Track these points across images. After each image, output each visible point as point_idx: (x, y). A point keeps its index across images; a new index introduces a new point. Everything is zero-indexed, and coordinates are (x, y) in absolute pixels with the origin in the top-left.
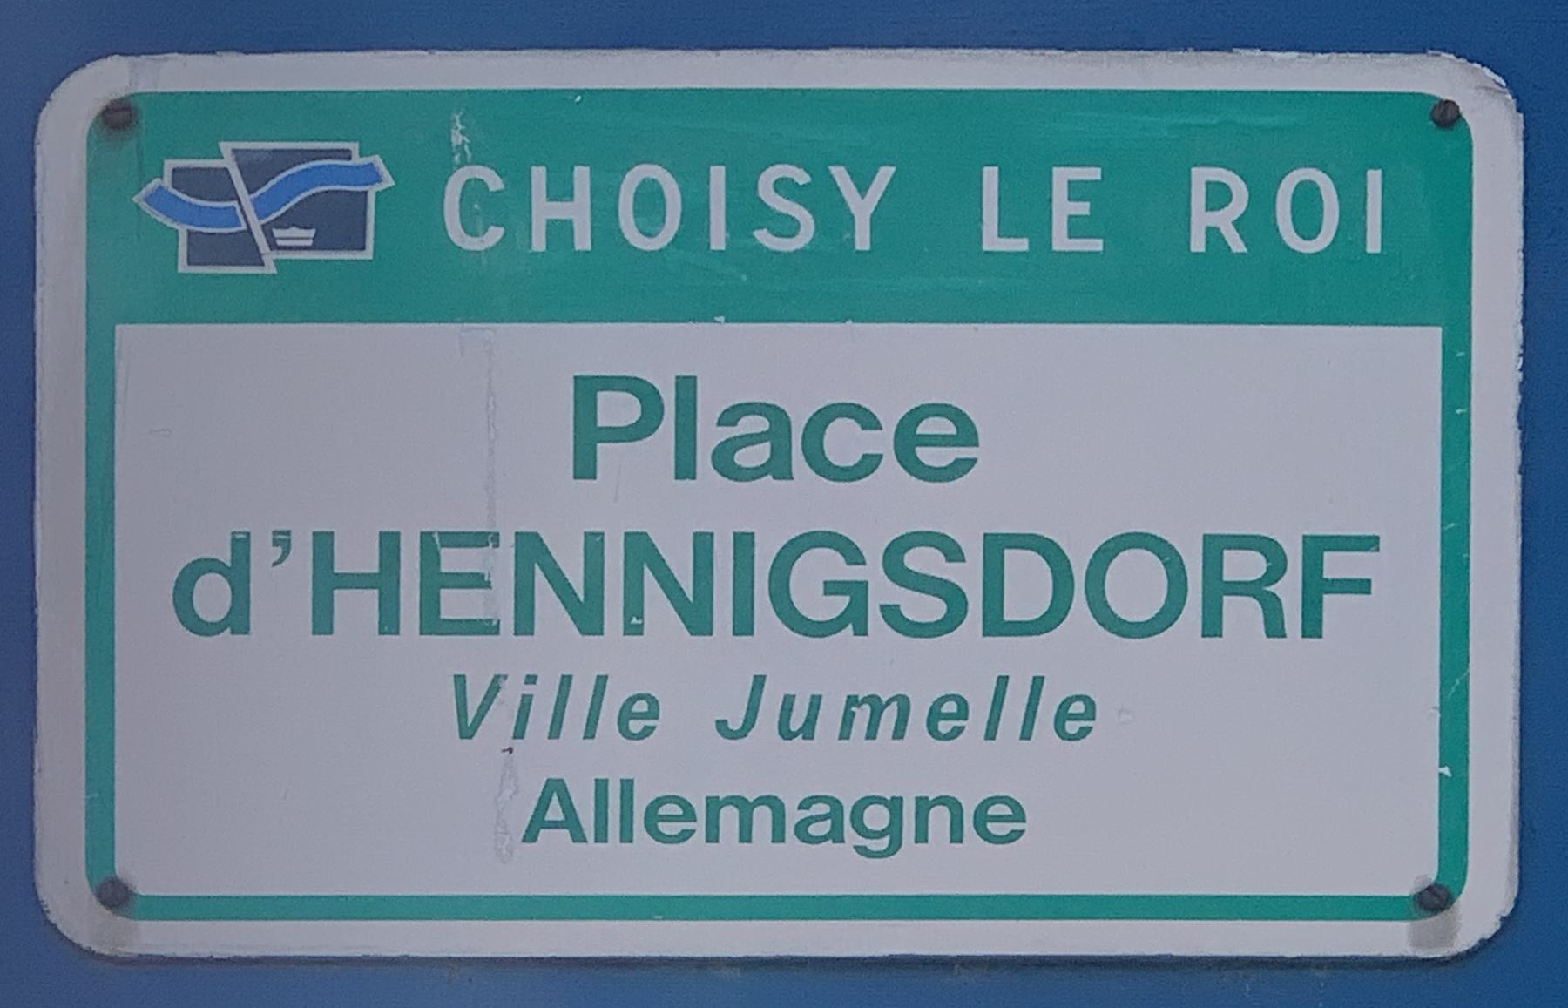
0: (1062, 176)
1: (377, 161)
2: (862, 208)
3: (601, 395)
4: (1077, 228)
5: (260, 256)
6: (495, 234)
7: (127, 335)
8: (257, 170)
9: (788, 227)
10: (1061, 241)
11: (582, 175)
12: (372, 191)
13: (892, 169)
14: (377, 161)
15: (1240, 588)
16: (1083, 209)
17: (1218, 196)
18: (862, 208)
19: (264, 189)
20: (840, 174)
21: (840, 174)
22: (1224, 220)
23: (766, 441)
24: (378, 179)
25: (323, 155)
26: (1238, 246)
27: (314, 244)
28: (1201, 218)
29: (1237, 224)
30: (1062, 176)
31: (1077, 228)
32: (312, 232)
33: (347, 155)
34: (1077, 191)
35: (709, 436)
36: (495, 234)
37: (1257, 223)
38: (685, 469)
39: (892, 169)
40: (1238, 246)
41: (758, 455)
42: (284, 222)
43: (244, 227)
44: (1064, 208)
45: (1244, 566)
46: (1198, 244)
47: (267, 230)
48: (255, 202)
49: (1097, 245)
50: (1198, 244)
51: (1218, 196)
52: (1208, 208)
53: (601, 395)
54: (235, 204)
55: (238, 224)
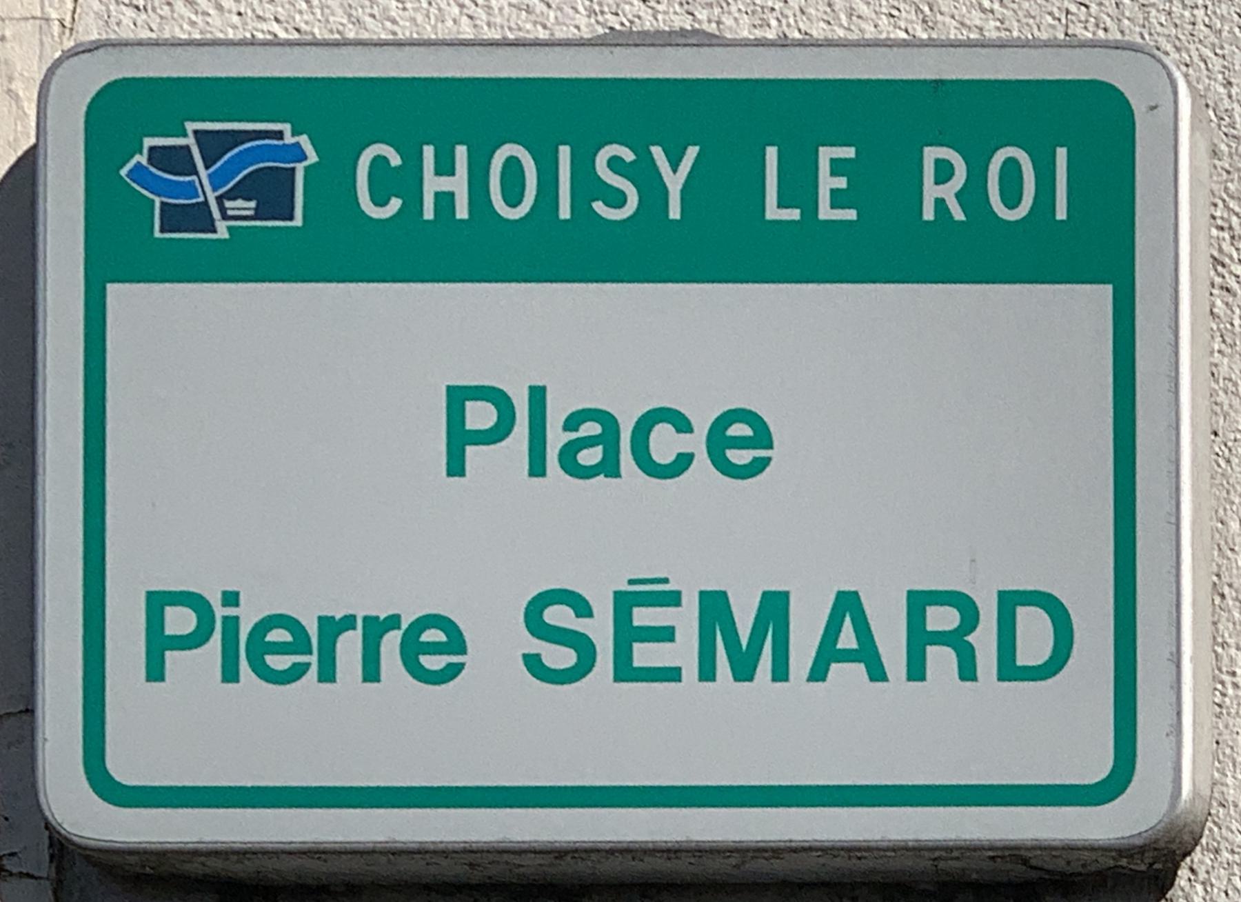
0: (826, 155)
1: (304, 140)
2: (675, 183)
3: (469, 405)
4: (837, 199)
5: (212, 221)
6: (395, 204)
7: (114, 290)
8: (214, 145)
9: (618, 200)
10: (826, 212)
11: (461, 151)
12: (300, 168)
13: (697, 148)
14: (304, 140)
15: (940, 638)
16: (841, 183)
17: (944, 172)
18: (675, 183)
19: (219, 164)
20: (657, 151)
21: (657, 151)
22: (949, 192)
23: (598, 445)
24: (305, 158)
25: (263, 135)
26: (959, 215)
27: (256, 213)
28: (931, 192)
29: (958, 195)
30: (826, 155)
31: (837, 199)
32: (253, 204)
33: (279, 135)
34: (837, 167)
35: (556, 439)
36: (395, 204)
37: (973, 194)
38: (537, 468)
39: (697, 148)
40: (959, 215)
41: (590, 457)
42: (232, 195)
43: (201, 199)
44: (828, 183)
45: (942, 619)
46: (929, 214)
47: (220, 199)
48: (210, 176)
49: (851, 215)
50: (929, 214)
51: (944, 172)
52: (937, 183)
53: (469, 405)
54: (194, 178)
55: (198, 196)
